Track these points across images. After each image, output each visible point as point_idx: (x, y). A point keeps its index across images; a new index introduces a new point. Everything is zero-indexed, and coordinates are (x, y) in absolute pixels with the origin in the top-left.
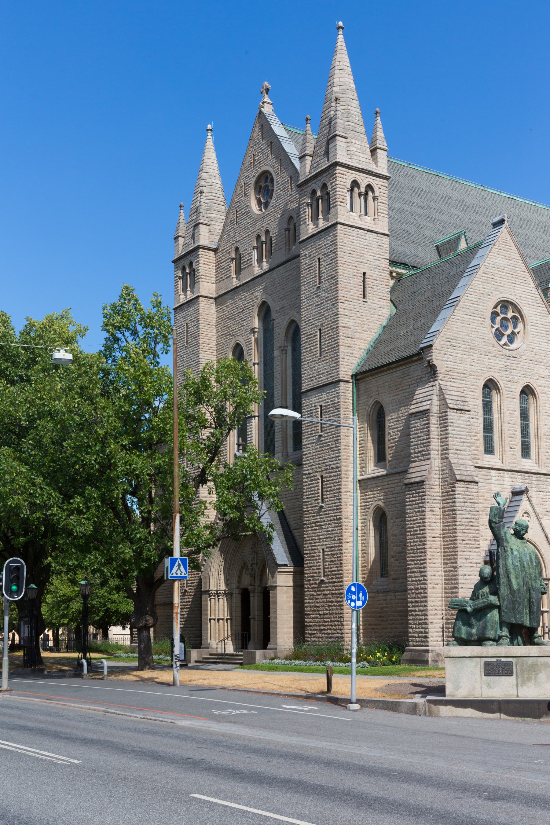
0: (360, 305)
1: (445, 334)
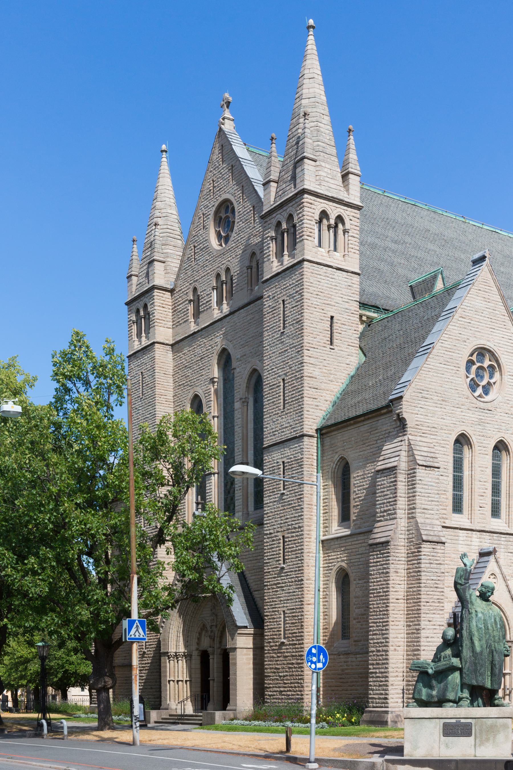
0: (327, 352)
1: (416, 385)
